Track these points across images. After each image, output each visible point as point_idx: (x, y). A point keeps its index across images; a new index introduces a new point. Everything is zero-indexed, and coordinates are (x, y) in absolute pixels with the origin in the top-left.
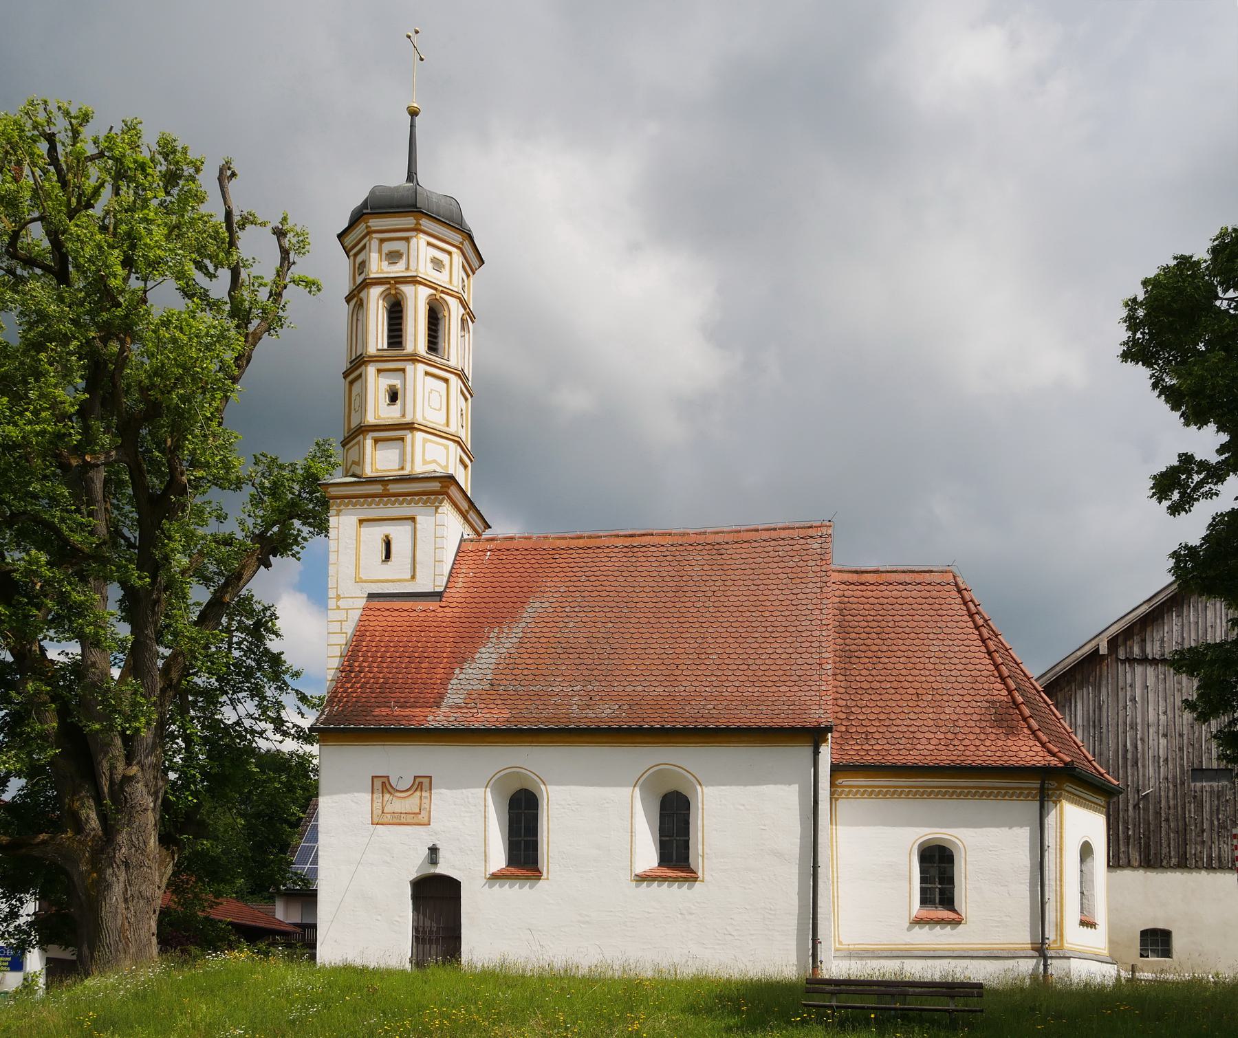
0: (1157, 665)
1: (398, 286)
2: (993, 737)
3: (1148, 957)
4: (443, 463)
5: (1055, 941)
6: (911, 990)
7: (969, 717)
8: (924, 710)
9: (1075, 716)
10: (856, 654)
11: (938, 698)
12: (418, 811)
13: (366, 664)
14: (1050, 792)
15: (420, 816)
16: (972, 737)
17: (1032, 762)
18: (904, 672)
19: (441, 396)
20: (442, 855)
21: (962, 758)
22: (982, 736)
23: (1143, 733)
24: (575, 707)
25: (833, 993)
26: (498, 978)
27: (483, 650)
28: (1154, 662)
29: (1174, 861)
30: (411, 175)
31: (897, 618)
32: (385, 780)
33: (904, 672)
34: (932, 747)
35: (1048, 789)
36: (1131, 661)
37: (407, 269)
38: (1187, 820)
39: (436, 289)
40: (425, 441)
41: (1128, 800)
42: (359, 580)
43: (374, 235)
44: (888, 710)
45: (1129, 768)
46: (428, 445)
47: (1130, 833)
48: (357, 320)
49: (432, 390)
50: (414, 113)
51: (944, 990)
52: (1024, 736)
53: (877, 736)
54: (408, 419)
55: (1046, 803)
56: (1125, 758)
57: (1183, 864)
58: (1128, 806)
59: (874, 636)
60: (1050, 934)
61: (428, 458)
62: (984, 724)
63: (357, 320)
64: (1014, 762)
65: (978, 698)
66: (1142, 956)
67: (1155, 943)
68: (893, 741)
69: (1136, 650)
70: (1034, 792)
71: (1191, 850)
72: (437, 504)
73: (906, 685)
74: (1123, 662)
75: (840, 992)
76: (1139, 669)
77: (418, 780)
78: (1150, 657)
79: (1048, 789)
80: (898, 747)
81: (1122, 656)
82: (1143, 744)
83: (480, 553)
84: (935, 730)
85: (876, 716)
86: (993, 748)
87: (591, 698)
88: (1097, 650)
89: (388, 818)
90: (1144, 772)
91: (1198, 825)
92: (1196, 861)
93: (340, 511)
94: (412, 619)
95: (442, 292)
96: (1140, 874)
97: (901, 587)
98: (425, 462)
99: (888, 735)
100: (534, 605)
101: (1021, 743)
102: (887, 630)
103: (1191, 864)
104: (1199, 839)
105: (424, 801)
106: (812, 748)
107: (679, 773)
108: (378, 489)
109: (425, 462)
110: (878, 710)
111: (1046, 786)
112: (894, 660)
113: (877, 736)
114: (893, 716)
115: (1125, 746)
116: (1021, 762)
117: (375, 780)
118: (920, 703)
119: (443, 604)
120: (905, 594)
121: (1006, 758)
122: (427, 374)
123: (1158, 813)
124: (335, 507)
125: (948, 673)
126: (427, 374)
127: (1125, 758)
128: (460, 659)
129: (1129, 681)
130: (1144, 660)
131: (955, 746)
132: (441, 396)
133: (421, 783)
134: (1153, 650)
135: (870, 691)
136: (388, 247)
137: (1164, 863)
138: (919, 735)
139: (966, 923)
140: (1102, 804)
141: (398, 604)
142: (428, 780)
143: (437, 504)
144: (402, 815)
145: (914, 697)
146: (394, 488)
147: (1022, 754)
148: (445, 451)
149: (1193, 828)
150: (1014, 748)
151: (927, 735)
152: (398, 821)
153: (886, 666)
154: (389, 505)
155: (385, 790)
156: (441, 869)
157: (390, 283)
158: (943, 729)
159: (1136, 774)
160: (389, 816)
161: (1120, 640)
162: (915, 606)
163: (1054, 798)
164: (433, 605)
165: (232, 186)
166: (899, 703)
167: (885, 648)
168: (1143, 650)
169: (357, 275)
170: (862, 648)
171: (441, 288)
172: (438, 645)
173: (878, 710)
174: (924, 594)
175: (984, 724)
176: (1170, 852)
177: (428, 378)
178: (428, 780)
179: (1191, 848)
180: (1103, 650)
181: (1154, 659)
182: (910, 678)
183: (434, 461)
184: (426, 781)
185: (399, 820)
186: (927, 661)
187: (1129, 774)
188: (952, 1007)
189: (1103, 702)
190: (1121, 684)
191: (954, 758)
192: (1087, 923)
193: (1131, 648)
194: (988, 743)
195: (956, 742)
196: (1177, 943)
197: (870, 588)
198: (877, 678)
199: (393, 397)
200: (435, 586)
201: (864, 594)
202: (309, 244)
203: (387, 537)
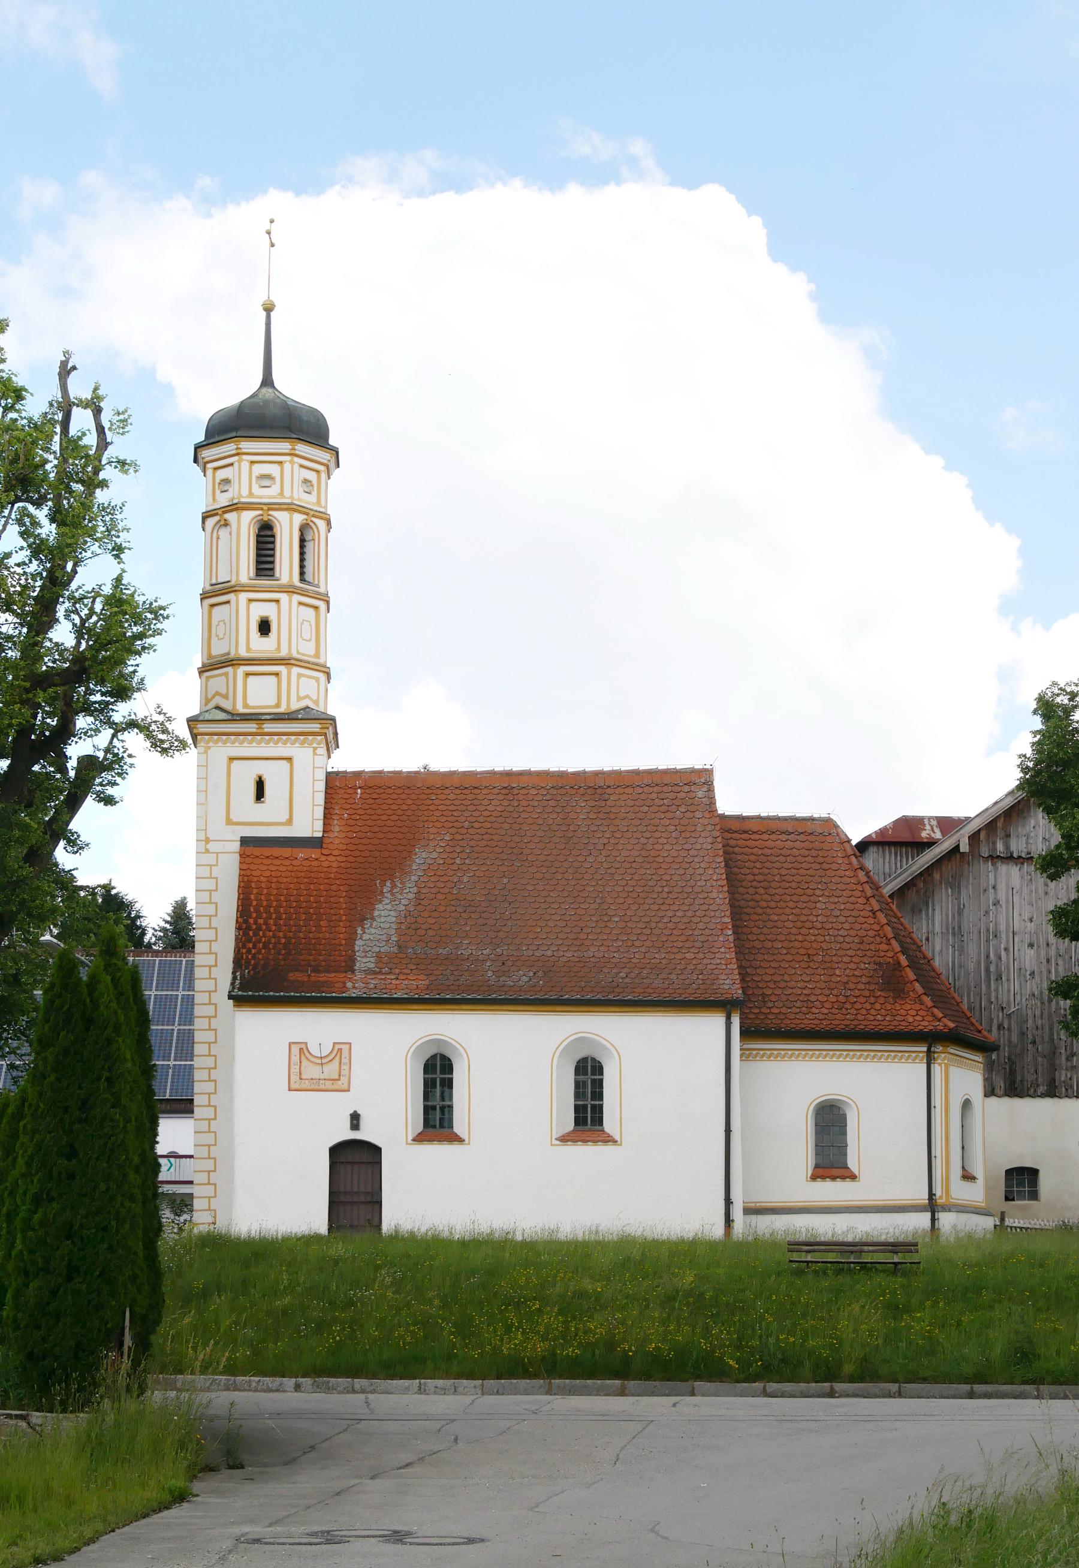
0: (1023, 863)
1: (271, 513)
2: (882, 1000)
3: (1013, 1200)
4: (315, 698)
5: (941, 1197)
6: (866, 1248)
7: (859, 979)
8: (816, 971)
9: (933, 920)
10: (746, 910)
11: (828, 959)
12: (337, 1077)
13: (261, 921)
14: (936, 1055)
15: (340, 1083)
16: (863, 1000)
17: (920, 1027)
18: (794, 931)
19: (311, 625)
20: (364, 1123)
21: (855, 1022)
22: (872, 1000)
23: (1008, 942)
24: (490, 974)
25: (808, 1252)
26: (396, 1237)
27: (380, 906)
28: (1019, 860)
29: (1042, 1089)
30: (267, 381)
31: (784, 872)
32: (303, 1046)
33: (794, 931)
34: (826, 1011)
35: (934, 1052)
36: (994, 858)
37: (282, 493)
38: (1055, 1042)
39: (307, 514)
40: (300, 675)
41: (992, 1020)
42: (229, 822)
43: (244, 457)
44: (782, 971)
45: (992, 982)
46: (302, 679)
47: (993, 1058)
48: (218, 538)
49: (303, 620)
50: (269, 309)
51: (890, 1248)
52: (911, 1000)
53: (773, 998)
54: (284, 653)
55: (932, 1065)
56: (987, 970)
57: (1052, 1092)
58: (991, 1027)
59: (762, 891)
60: (938, 1191)
61: (302, 694)
62: (872, 987)
63: (218, 538)
64: (903, 1027)
65: (866, 960)
66: (1007, 1199)
67: (1021, 1184)
68: (788, 1004)
69: (1000, 847)
70: (921, 1055)
71: (1062, 1076)
72: (315, 745)
73: (797, 944)
74: (986, 859)
75: (814, 1251)
76: (1003, 868)
77: (338, 1046)
78: (1015, 855)
79: (934, 1052)
80: (794, 1010)
81: (985, 852)
82: (1007, 955)
83: (350, 791)
84: (828, 992)
85: (770, 977)
86: (883, 1012)
87: (503, 963)
88: (957, 847)
89: (306, 1084)
90: (1009, 986)
91: (1068, 1048)
92: (1067, 1090)
93: (209, 748)
94: (295, 869)
95: (314, 516)
96: (1006, 1101)
97: (784, 837)
98: (299, 698)
99: (784, 998)
100: (421, 857)
101: (909, 1007)
102: (774, 885)
103: (1061, 1093)
104: (1069, 1064)
105: (343, 1067)
106: (725, 1018)
107: (603, 1045)
108: (251, 727)
109: (299, 698)
110: (772, 971)
111: (932, 1049)
112: (783, 918)
113: (773, 998)
114: (787, 978)
115: (988, 957)
116: (910, 1027)
117: (292, 1046)
118: (811, 964)
119: (325, 852)
120: (788, 844)
121: (895, 1023)
122: (300, 603)
123: (1022, 1034)
124: (202, 744)
125: (836, 933)
126: (300, 603)
127: (987, 970)
128: (360, 916)
129: (992, 882)
130: (1010, 858)
131: (847, 1009)
132: (311, 625)
133: (340, 1050)
134: (1018, 846)
135: (762, 951)
136: (258, 470)
137: (1032, 1092)
138: (813, 998)
139: (859, 1181)
140: (980, 1060)
141: (277, 851)
142: (348, 1046)
143: (315, 745)
144: (321, 1081)
145: (806, 958)
146: (269, 727)
147: (911, 1019)
148: (317, 684)
149: (1063, 1051)
150: (903, 1012)
151: (820, 998)
152: (316, 1087)
153: (776, 924)
154: (263, 745)
155: (303, 1057)
156: (364, 1134)
157: (262, 509)
158: (835, 992)
159: (1000, 988)
160: (307, 1082)
161: (982, 836)
162: (799, 859)
163: (939, 1061)
164: (315, 854)
165: (71, 380)
166: (792, 964)
167: (773, 904)
168: (1007, 847)
169: (218, 492)
170: (750, 904)
171: (312, 513)
172: (332, 899)
173: (772, 971)
174: (807, 845)
175: (872, 987)
176: (1037, 1079)
177: (302, 608)
178: (348, 1046)
179: (1060, 1074)
180: (964, 848)
181: (1020, 857)
182: (800, 938)
183: (307, 697)
184: (345, 1048)
185: (316, 1086)
186: (815, 919)
187: (992, 990)
188: (896, 1260)
189: (964, 905)
190: (983, 885)
191: (848, 1023)
192: (968, 1177)
193: (994, 843)
194: (878, 1006)
195: (848, 1006)
196: (1046, 1184)
197: (753, 837)
198: (769, 937)
199: (264, 627)
200: (313, 831)
201: (748, 843)
202: (131, 424)
203: (260, 778)
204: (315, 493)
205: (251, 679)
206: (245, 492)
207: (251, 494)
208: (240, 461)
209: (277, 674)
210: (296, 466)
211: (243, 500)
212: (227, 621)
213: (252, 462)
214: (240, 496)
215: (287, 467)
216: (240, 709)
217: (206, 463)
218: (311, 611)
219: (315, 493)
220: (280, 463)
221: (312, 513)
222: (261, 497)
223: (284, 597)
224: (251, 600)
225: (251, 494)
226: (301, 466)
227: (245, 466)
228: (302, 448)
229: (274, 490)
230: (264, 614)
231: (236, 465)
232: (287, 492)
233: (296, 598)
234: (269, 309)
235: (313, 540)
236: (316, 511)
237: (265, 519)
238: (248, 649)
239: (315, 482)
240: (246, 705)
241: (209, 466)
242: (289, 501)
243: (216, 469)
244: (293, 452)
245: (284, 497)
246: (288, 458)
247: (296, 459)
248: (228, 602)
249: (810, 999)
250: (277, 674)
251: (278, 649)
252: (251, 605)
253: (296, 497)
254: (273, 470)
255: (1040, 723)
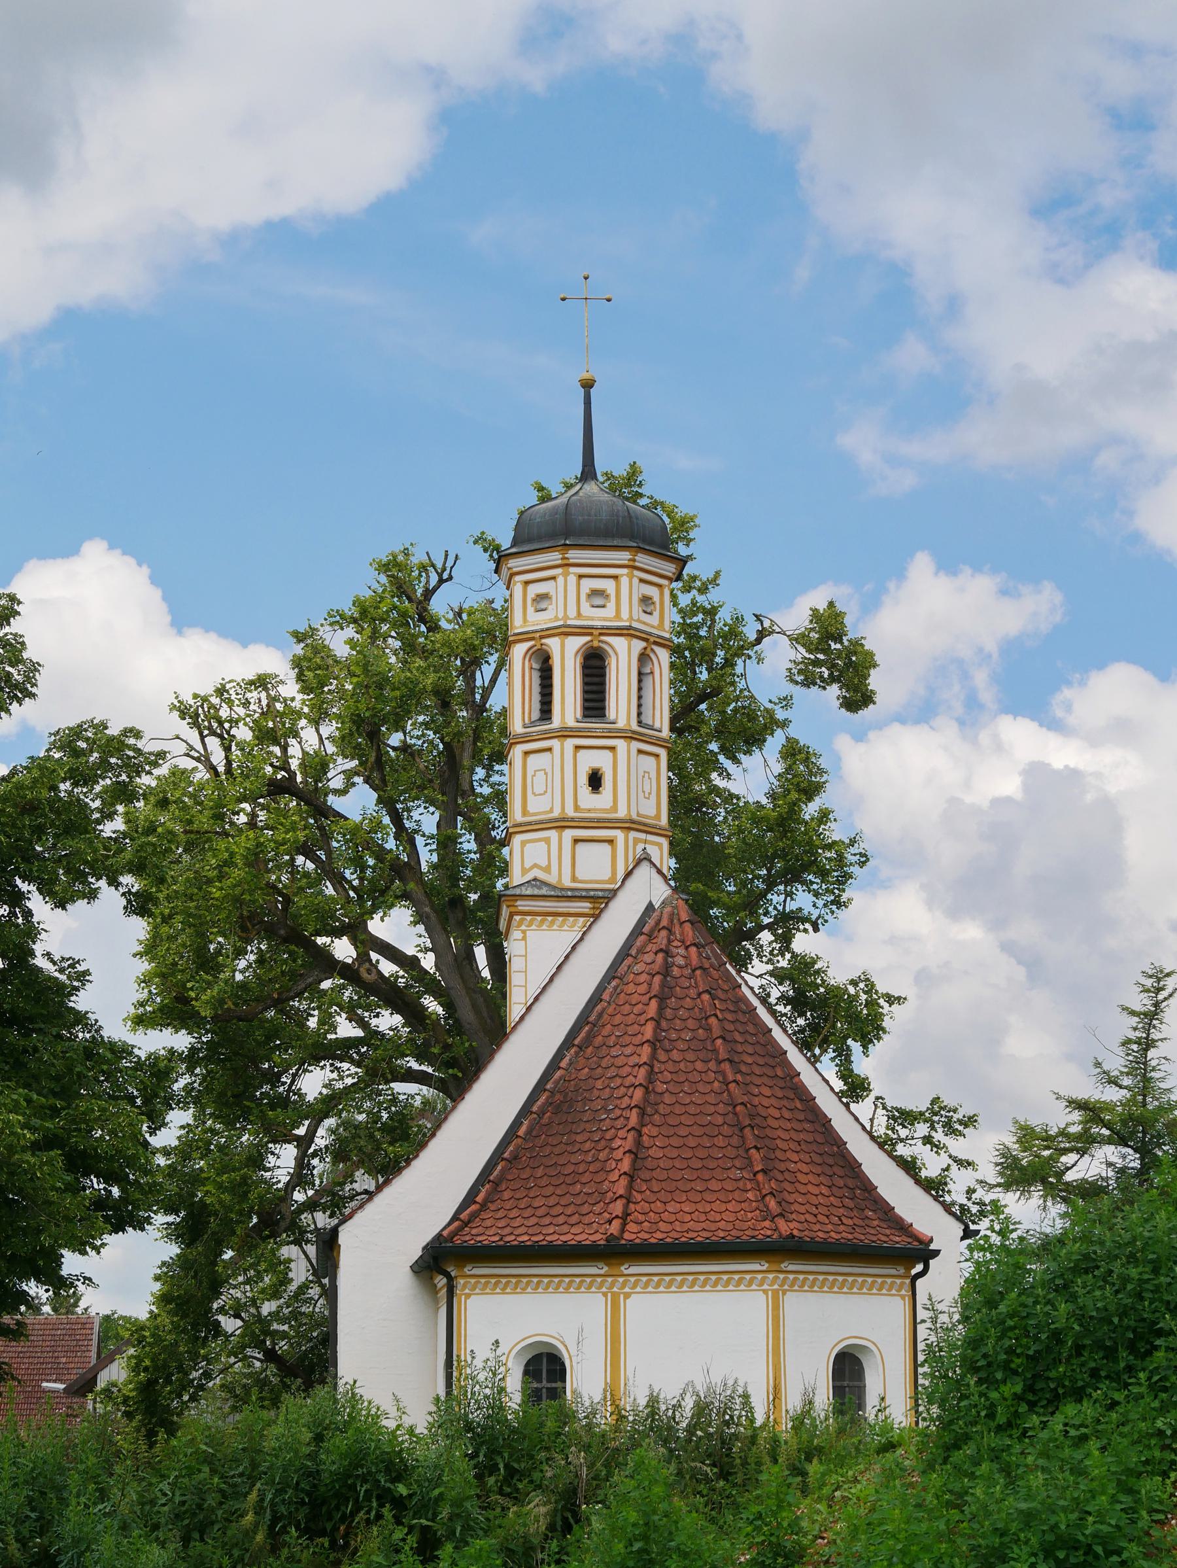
50: (588, 385)
122: (640, 752)
126: (640, 752)
169: (530, 609)
177: (642, 756)
204: (656, 614)
205: (581, 847)
206: (572, 612)
207: (579, 615)
208: (566, 575)
209: (611, 842)
210: (635, 581)
211: (569, 622)
212: (641, 795)
213: (581, 577)
214: (566, 617)
215: (624, 581)
216: (567, 882)
217: (512, 575)
218: (652, 759)
219: (656, 614)
220: (615, 577)
221: (538, 635)
222: (592, 619)
223: (620, 744)
224: (578, 748)
225: (579, 615)
226: (642, 581)
227: (572, 579)
228: (643, 560)
229: (610, 611)
230: (596, 765)
231: (560, 580)
232: (625, 615)
233: (636, 745)
234: (588, 385)
235: (652, 673)
236: (542, 630)
237: (596, 644)
238: (577, 808)
239: (656, 599)
240: (574, 879)
241: (518, 578)
242: (627, 624)
243: (527, 583)
244: (565, 562)
245: (622, 620)
246: (625, 571)
247: (636, 573)
248: (549, 750)
249: (683, 1036)
250: (611, 842)
251: (615, 808)
252: (578, 755)
253: (635, 617)
254: (608, 586)
255: (766, 788)
